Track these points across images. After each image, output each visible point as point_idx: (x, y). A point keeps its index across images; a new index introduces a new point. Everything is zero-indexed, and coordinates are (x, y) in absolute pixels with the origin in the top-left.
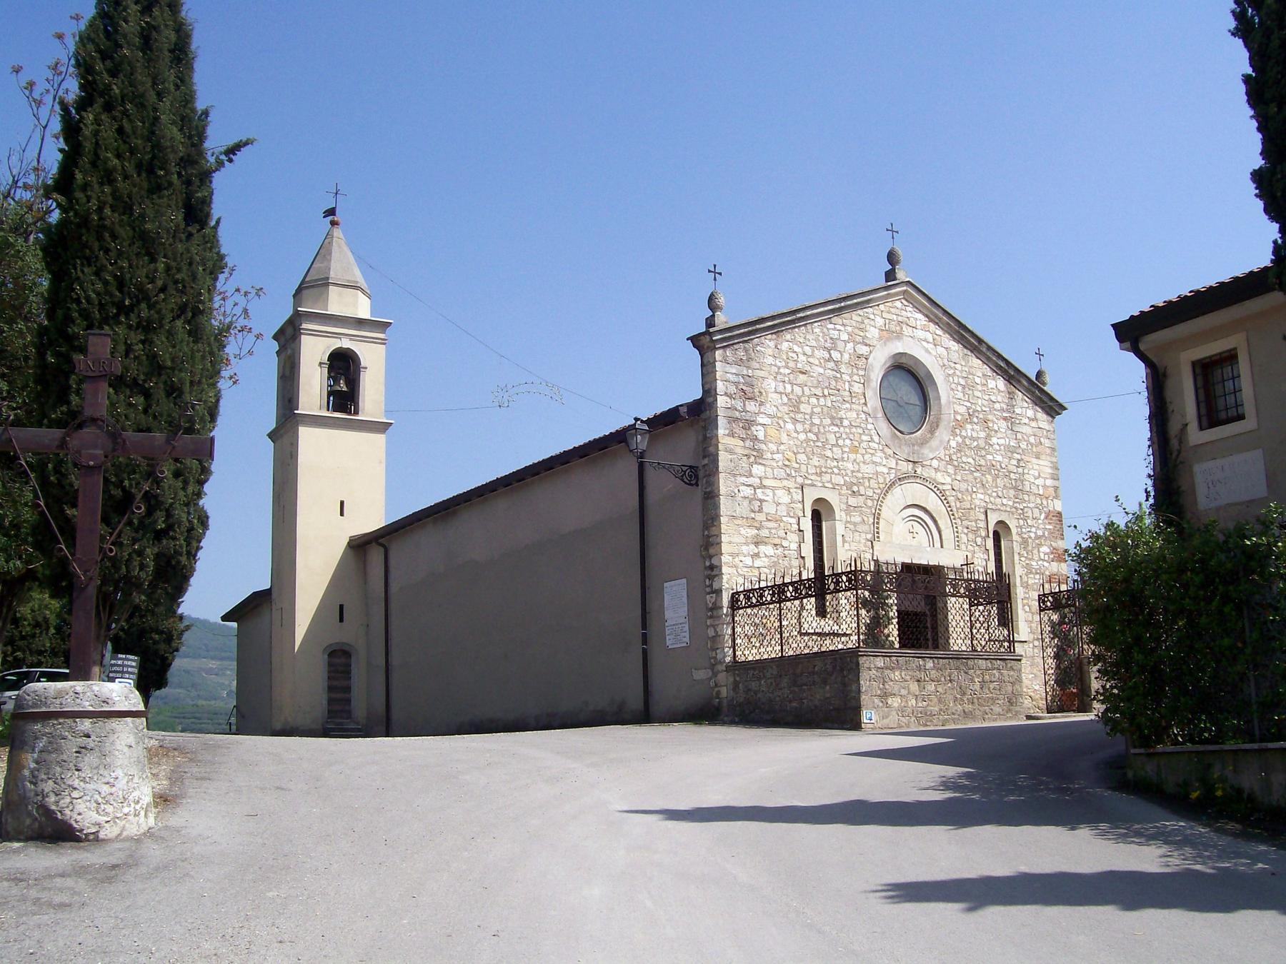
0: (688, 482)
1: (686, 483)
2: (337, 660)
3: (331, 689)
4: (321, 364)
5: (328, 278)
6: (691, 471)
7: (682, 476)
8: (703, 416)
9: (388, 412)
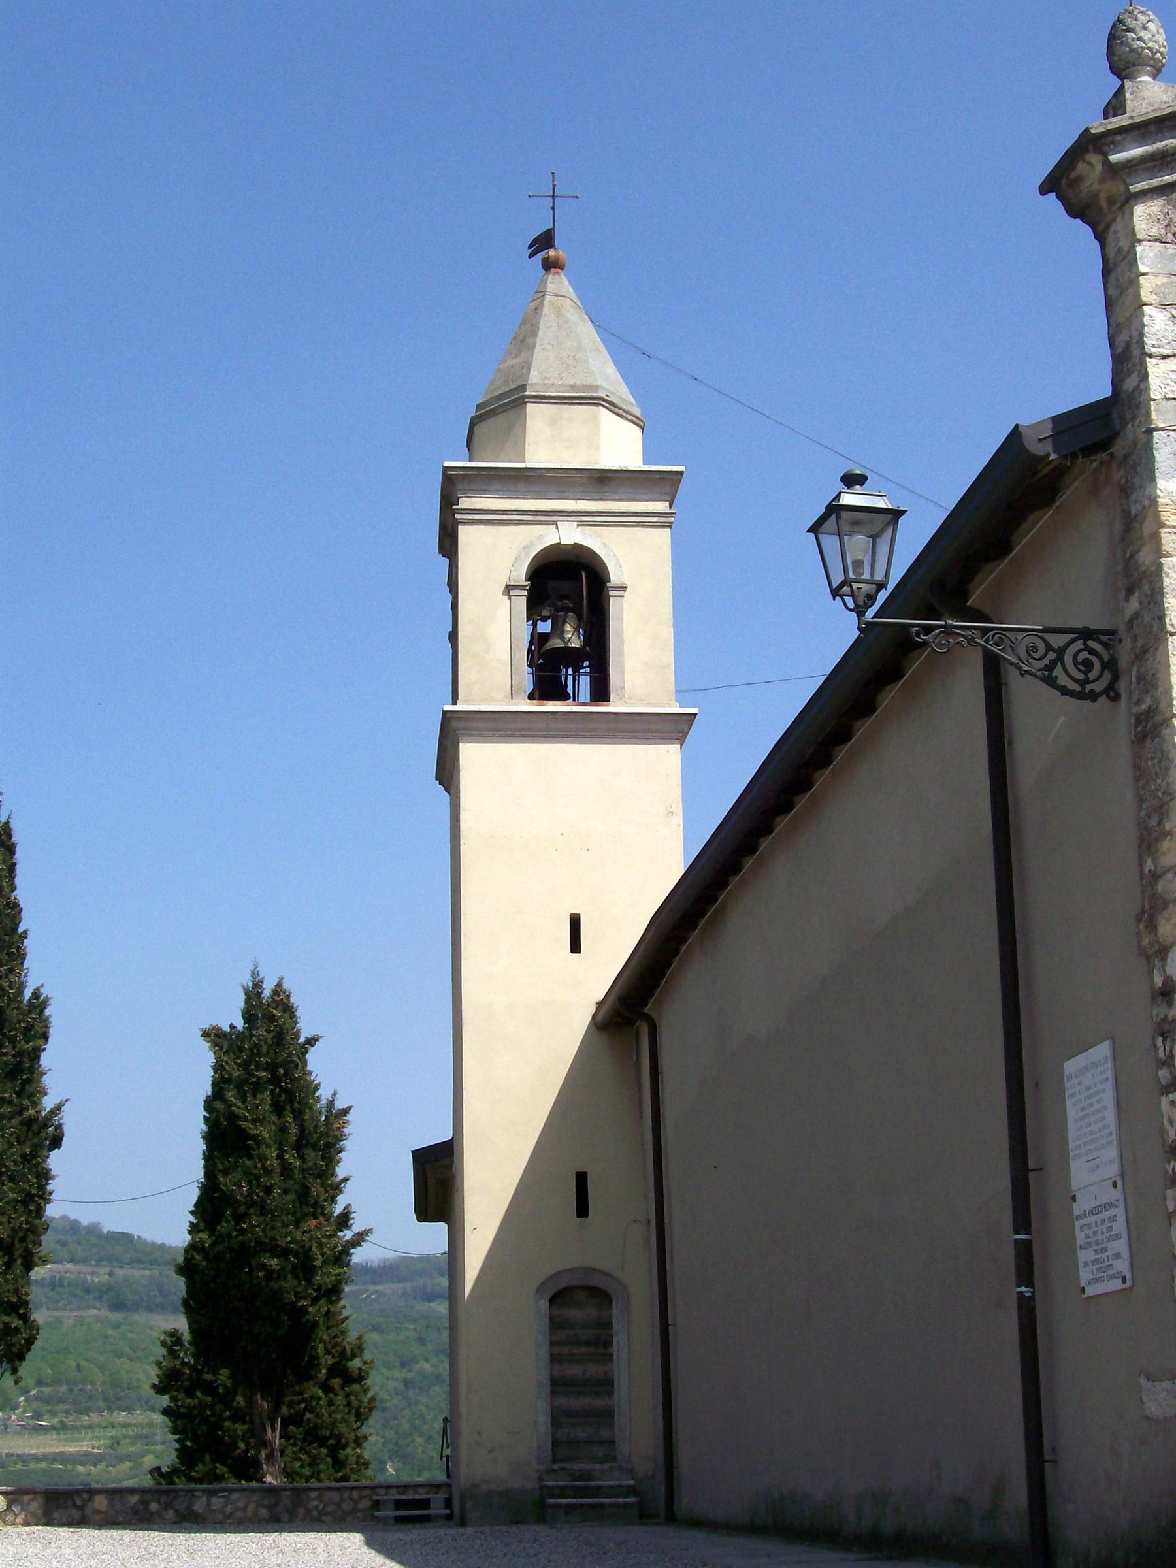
0: (1077, 688)
1: (1064, 691)
2: (574, 1314)
3: (558, 1385)
4: (509, 588)
5: (523, 387)
6: (1087, 649)
7: (1050, 667)
8: (1118, 448)
9: (681, 693)
